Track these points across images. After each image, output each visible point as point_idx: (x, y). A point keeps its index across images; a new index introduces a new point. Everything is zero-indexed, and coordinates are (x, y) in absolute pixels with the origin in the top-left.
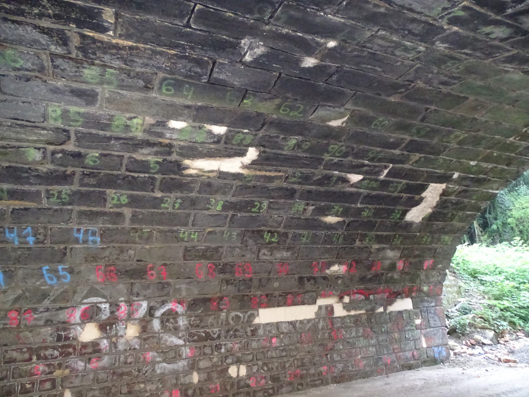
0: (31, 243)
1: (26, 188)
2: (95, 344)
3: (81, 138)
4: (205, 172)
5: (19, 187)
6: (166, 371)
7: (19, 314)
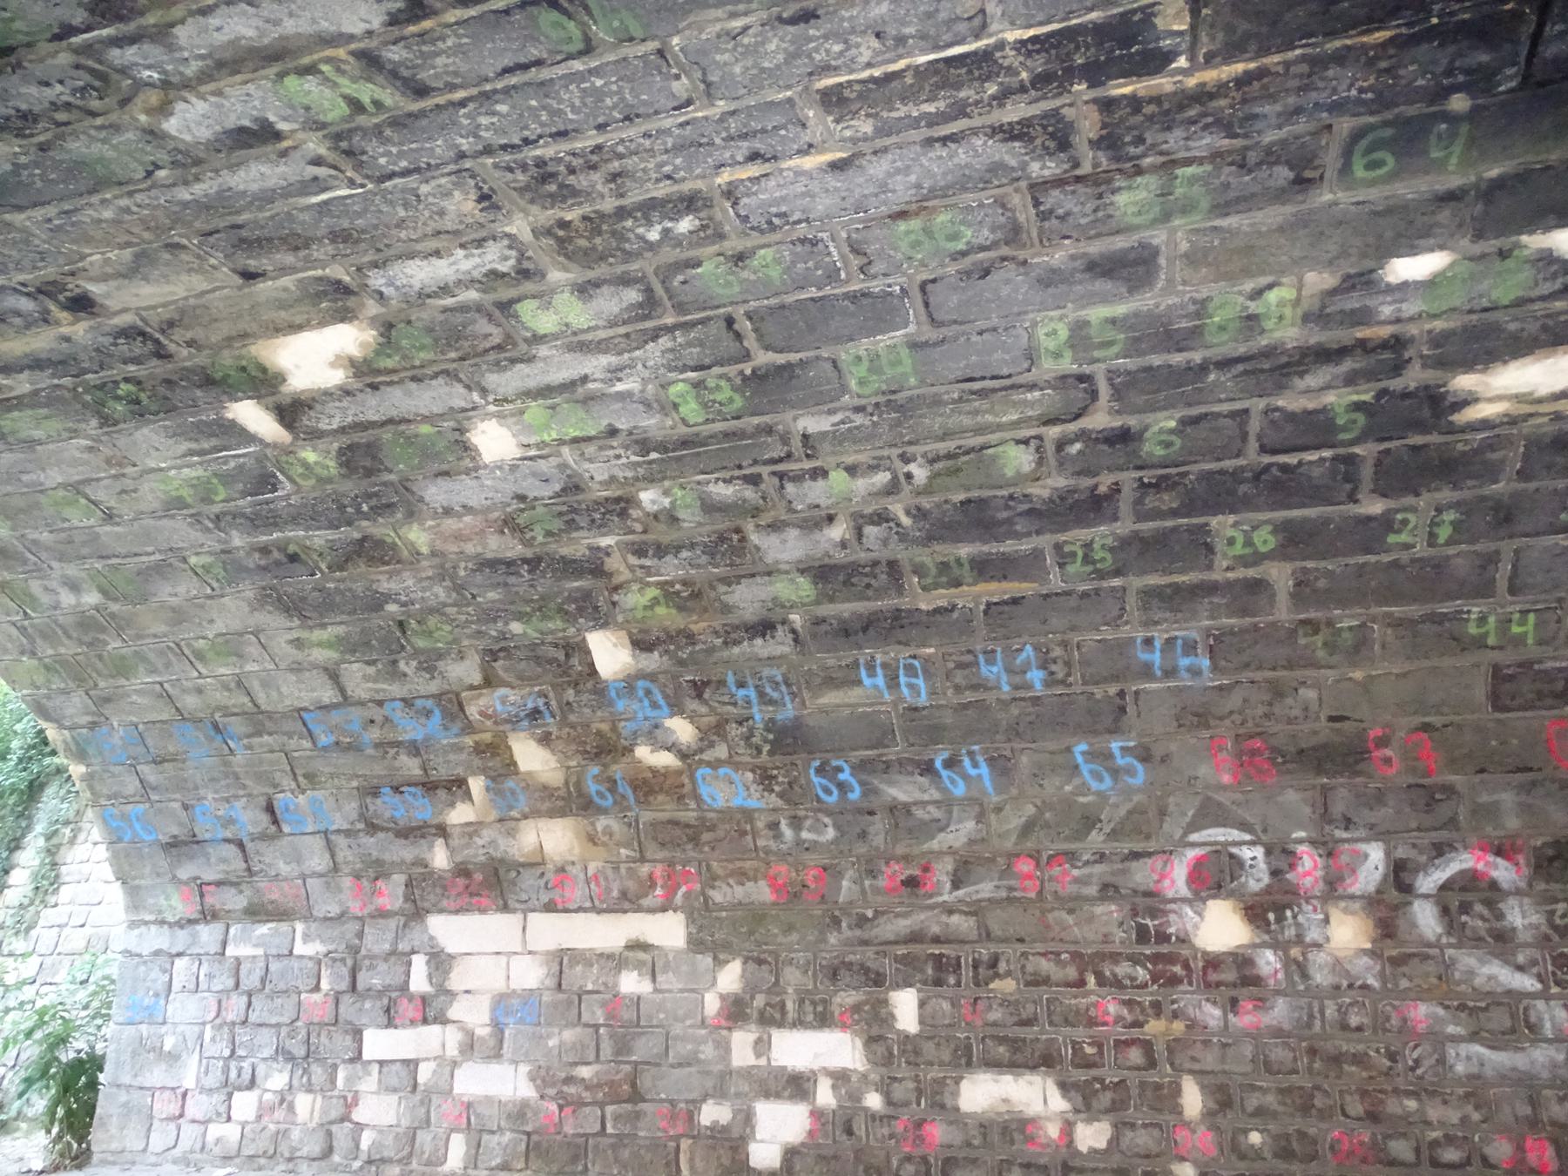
0: (1038, 685)
1: (1008, 546)
2: (1241, 960)
3: (1125, 387)
4: (1540, 401)
5: (993, 548)
6: (1489, 1072)
7: (1038, 865)
